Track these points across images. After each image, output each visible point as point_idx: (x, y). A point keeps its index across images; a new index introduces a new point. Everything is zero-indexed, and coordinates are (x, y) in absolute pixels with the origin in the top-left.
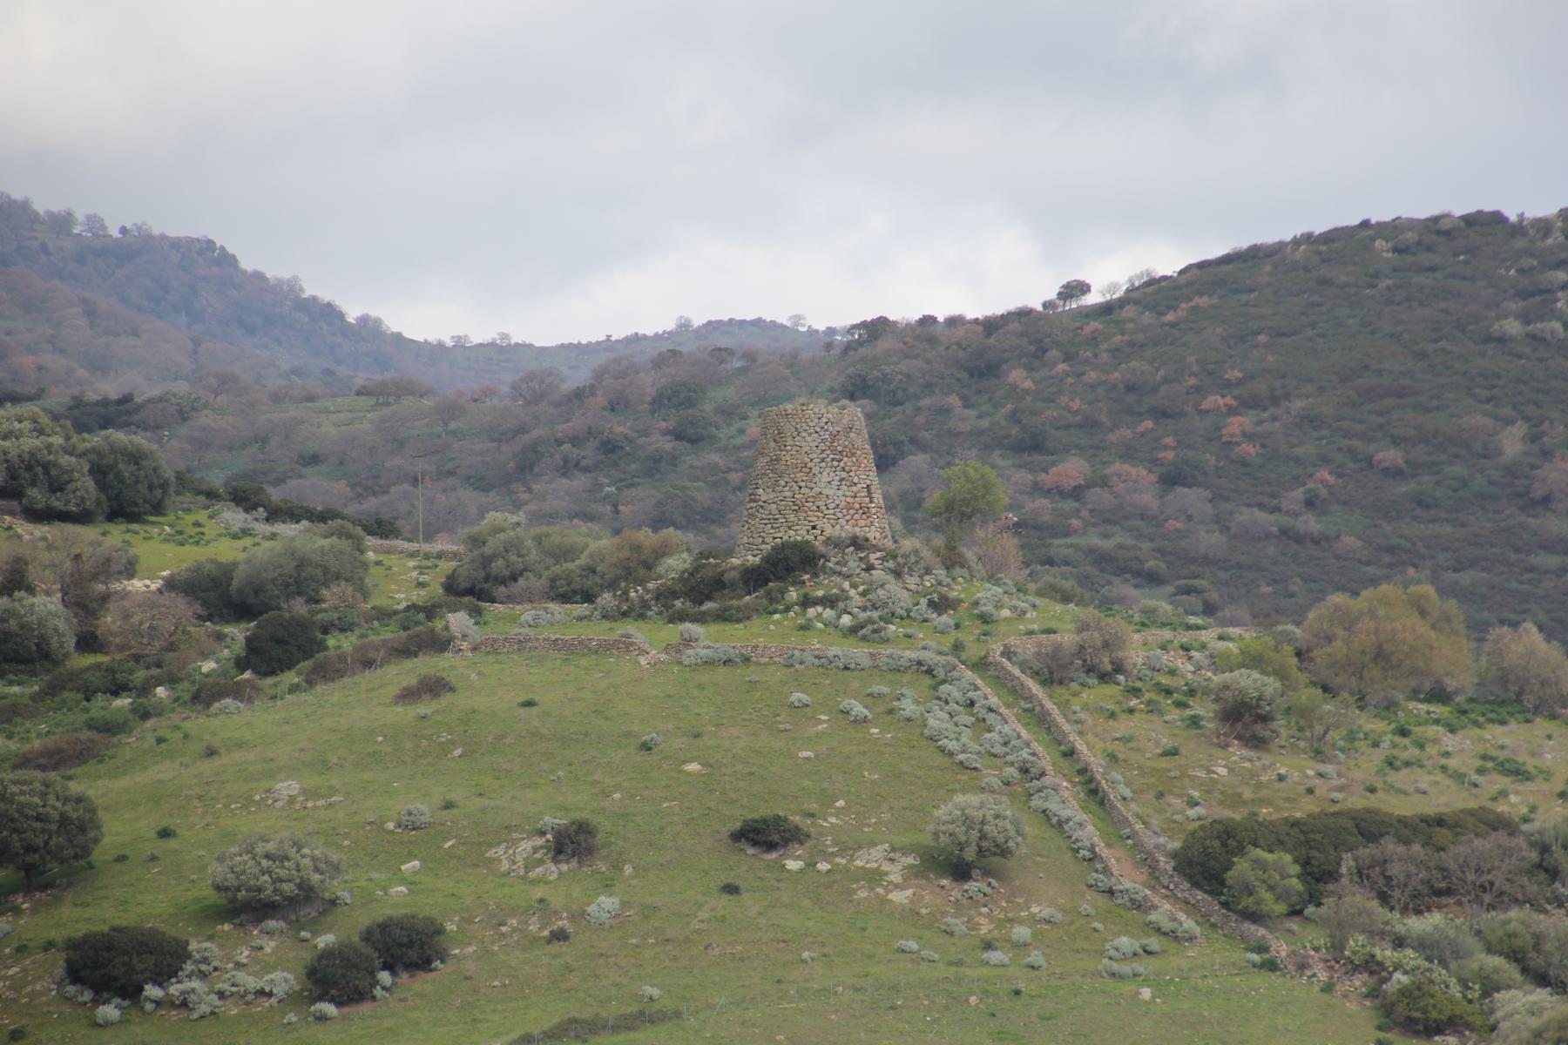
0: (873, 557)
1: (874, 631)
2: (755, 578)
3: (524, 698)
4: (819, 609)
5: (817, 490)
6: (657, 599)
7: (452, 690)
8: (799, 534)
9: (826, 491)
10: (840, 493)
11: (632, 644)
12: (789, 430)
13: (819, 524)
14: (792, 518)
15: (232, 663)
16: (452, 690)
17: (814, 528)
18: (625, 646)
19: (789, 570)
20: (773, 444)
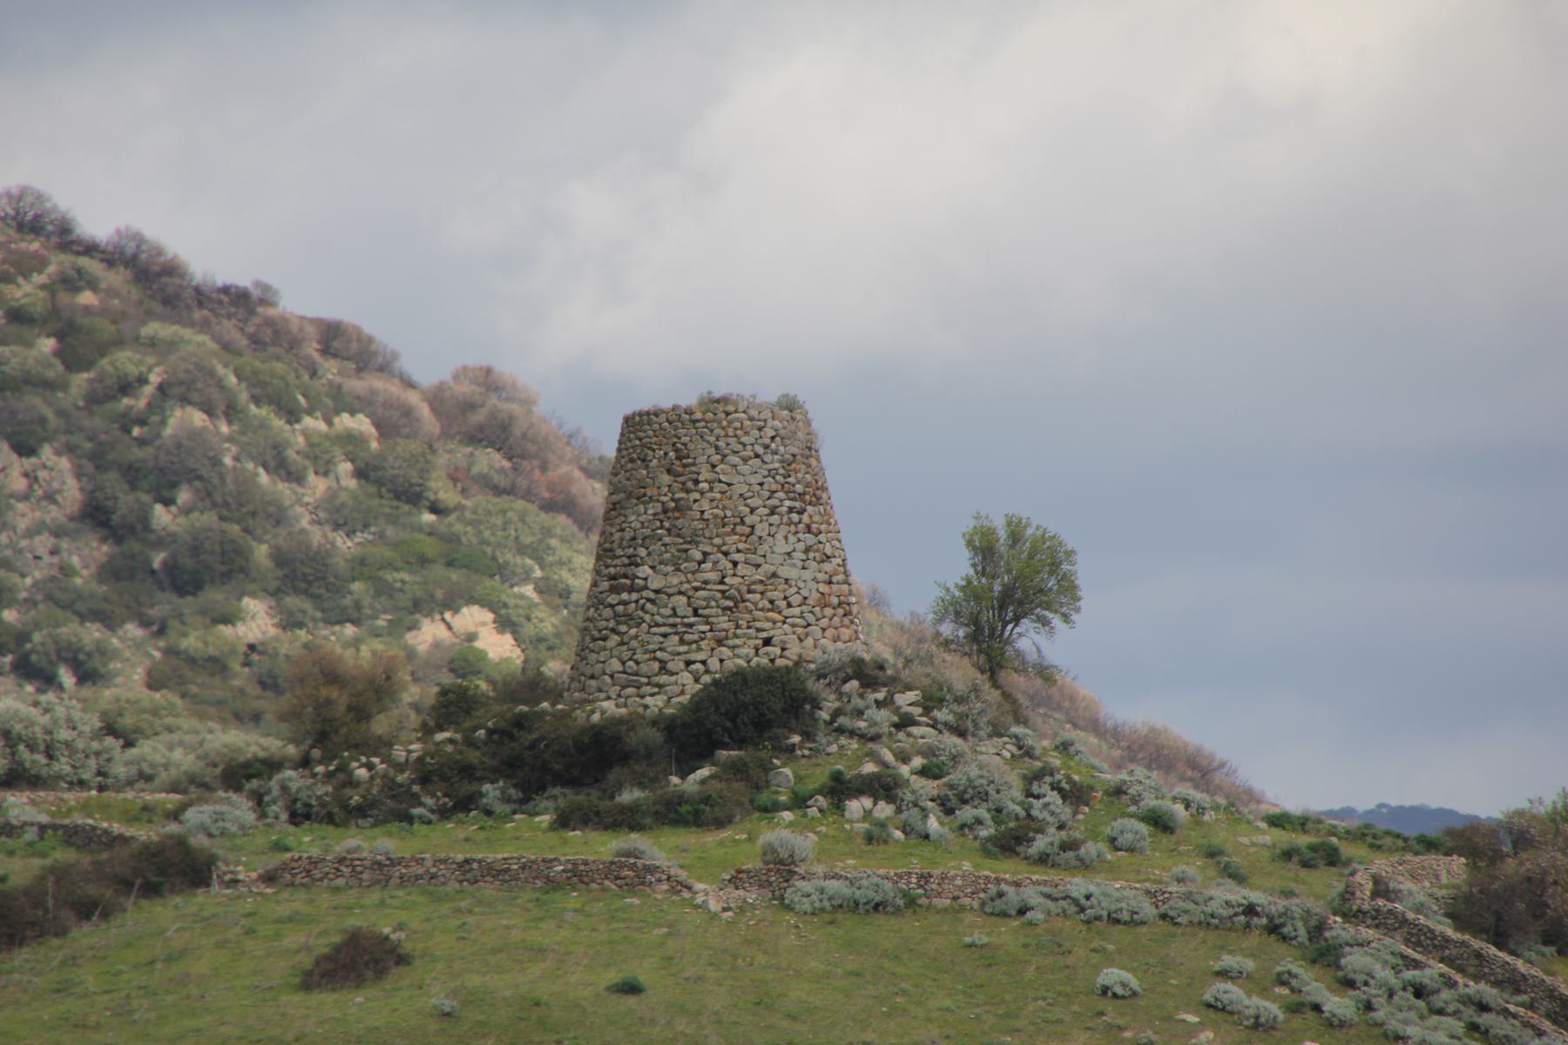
0: (905, 699)
1: (1066, 847)
2: (691, 737)
3: (613, 977)
4: (867, 802)
5: (767, 568)
6: (425, 779)
7: (402, 960)
8: (741, 655)
9: (784, 572)
10: (807, 575)
11: (651, 870)
12: (703, 454)
13: (777, 634)
14: (723, 622)
15: (947, 820)
16: (402, 960)
17: (767, 642)
18: (633, 875)
19: (762, 725)
20: (666, 479)
